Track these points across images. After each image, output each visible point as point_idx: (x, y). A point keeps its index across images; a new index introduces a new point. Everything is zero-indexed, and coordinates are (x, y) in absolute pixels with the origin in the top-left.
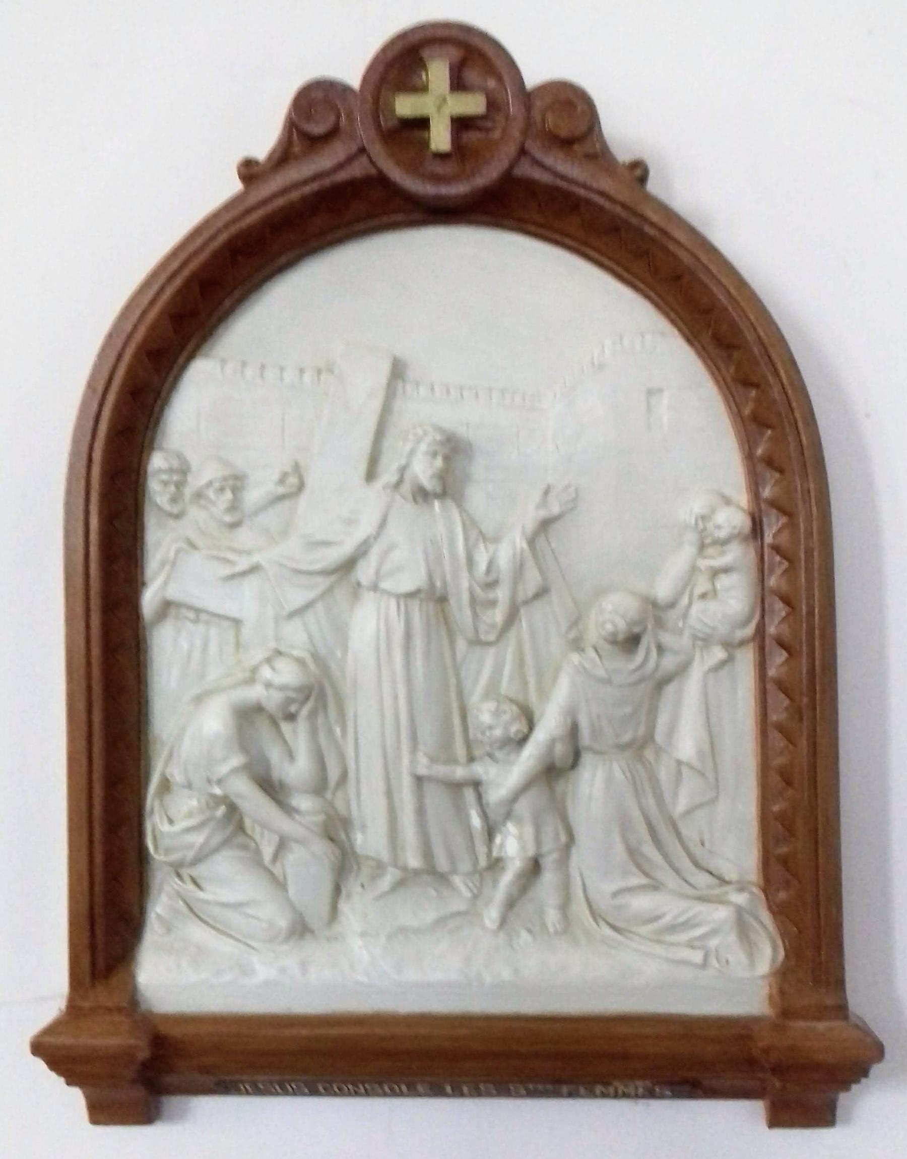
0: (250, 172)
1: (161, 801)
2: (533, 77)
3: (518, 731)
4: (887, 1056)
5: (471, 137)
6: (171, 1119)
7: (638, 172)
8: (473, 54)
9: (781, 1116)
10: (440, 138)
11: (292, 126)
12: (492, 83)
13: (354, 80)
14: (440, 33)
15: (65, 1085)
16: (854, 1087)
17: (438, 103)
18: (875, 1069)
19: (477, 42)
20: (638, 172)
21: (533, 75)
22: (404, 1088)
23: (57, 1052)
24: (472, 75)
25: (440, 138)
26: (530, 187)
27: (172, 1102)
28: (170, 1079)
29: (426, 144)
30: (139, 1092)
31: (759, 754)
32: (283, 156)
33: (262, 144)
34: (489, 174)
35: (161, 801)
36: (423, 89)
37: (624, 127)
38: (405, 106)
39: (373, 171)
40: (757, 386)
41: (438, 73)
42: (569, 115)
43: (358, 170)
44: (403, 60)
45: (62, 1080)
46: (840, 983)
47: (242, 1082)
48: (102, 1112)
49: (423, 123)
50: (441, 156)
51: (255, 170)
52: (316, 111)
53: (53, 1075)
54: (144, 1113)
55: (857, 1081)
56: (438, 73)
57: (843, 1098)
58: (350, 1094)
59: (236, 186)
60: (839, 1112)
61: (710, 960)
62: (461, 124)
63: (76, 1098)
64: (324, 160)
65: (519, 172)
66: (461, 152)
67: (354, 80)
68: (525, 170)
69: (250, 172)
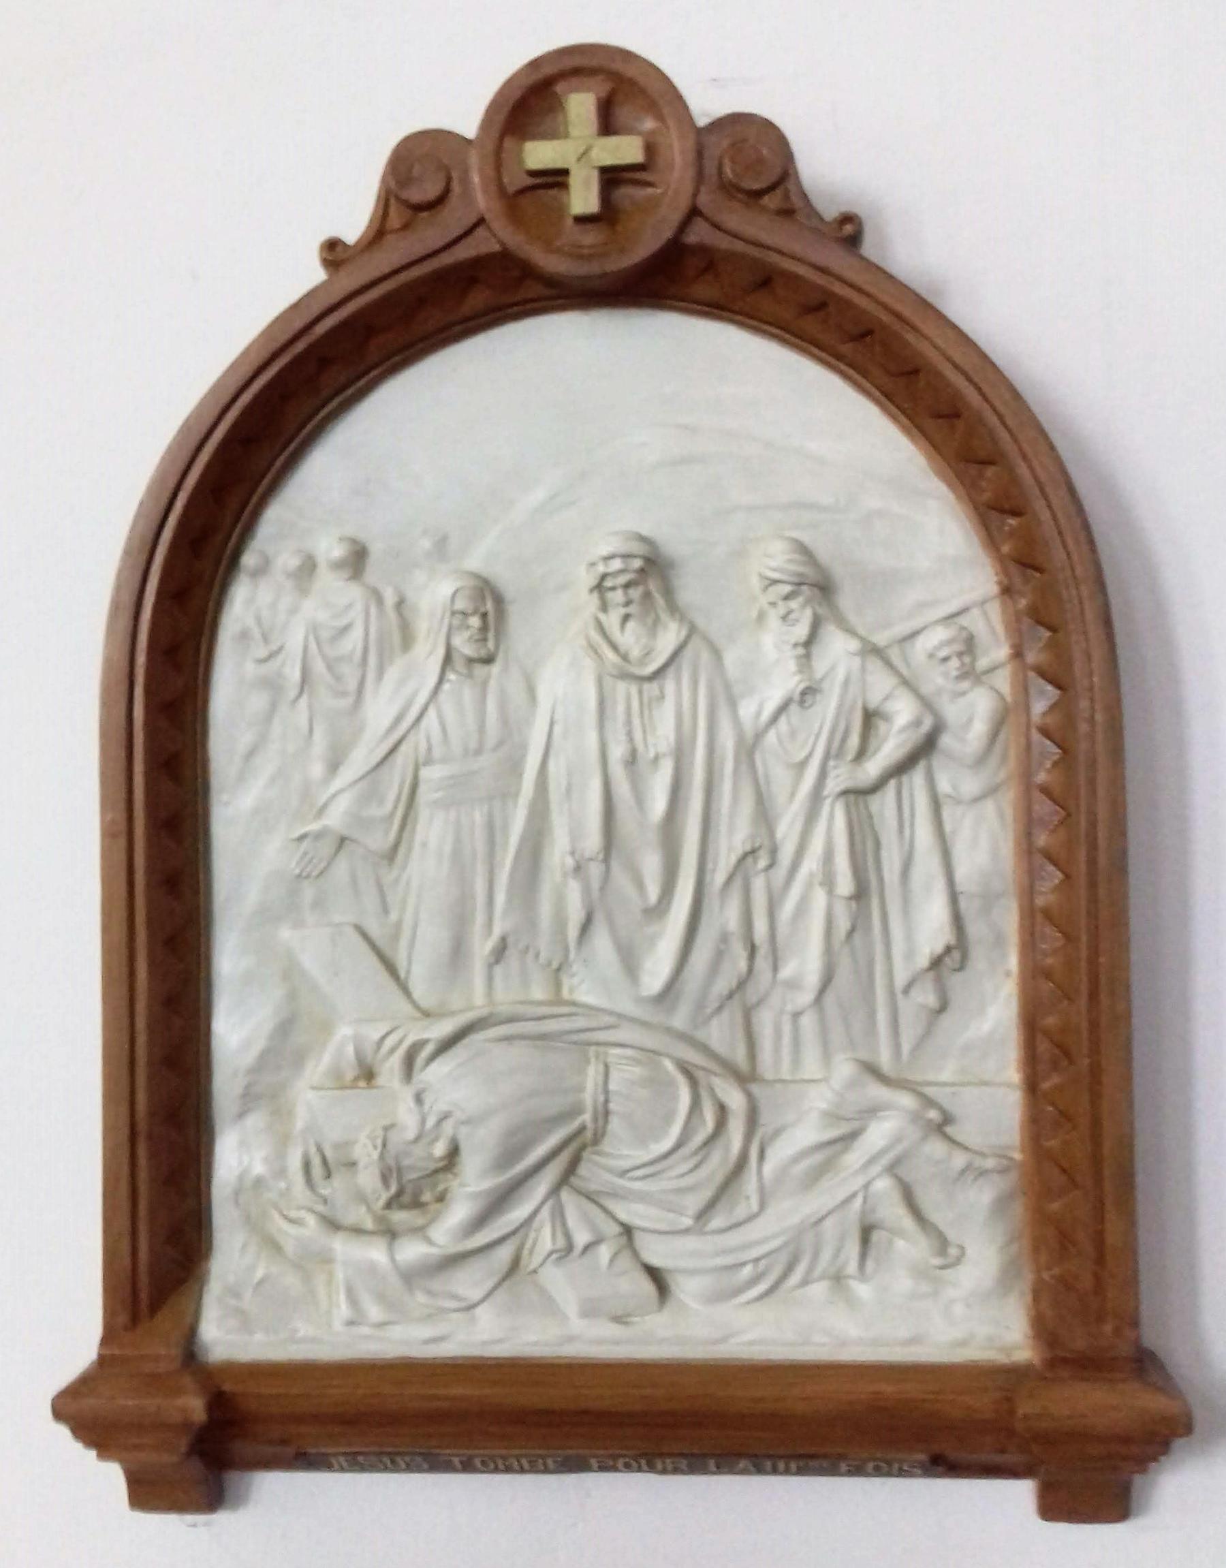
3: (266, 1160)
4: (1198, 1428)
6: (1137, 1515)
7: (849, 229)
8: (622, 84)
9: (1059, 1504)
11: (387, 199)
12: (649, 124)
13: (468, 124)
14: (577, 61)
17: (577, 148)
18: (1178, 1443)
19: (630, 71)
21: (706, 103)
22: (524, 1462)
23: (88, 1413)
24: (623, 114)
25: (583, 197)
26: (703, 250)
27: (233, 1478)
28: (241, 1448)
29: (561, 209)
31: (1137, 977)
32: (378, 234)
33: (353, 225)
34: (645, 243)
37: (830, 166)
38: (540, 154)
40: (1016, 513)
41: (580, 106)
42: (752, 160)
44: (529, 102)
45: (92, 1454)
47: (335, 1455)
48: (147, 1492)
49: (556, 178)
51: (340, 253)
52: (419, 175)
54: (211, 1497)
56: (580, 106)
57: (1138, 1480)
58: (385, 1469)
59: (318, 275)
60: (1134, 1505)
61: (958, 1305)
62: (612, 177)
63: (110, 1478)
64: (430, 235)
66: (607, 216)
67: (468, 124)
68: (699, 234)
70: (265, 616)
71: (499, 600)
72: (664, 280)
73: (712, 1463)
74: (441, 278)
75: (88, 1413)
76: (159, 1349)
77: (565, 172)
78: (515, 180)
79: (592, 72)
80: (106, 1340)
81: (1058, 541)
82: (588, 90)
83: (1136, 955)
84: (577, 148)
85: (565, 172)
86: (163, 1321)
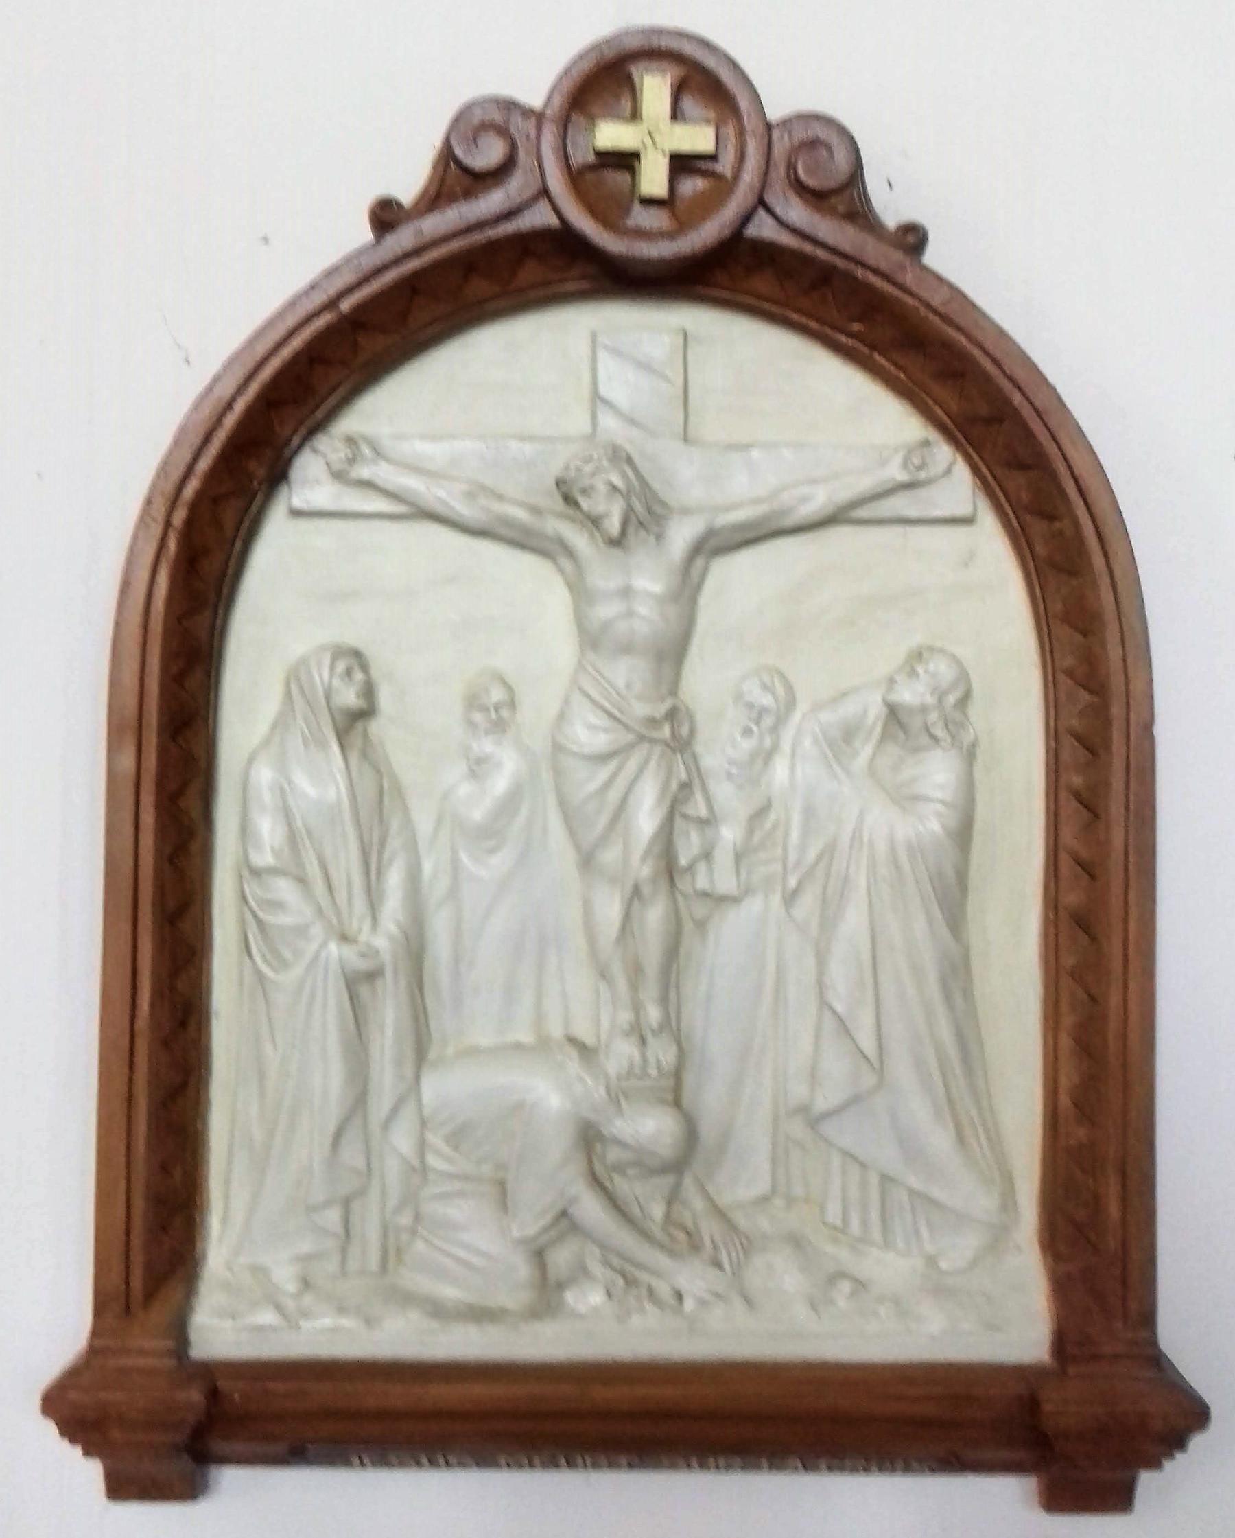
0: (385, 216)
1: (766, 896)
2: (774, 112)
5: (691, 186)
7: (911, 239)
8: (705, 81)
10: (653, 178)
13: (535, 98)
15: (1174, 1462)
16: (1168, 1465)
17: (654, 130)
20: (912, 239)
21: (779, 104)
23: (79, 1409)
25: (653, 178)
28: (218, 1446)
30: (185, 1463)
34: (708, 233)
35: (766, 896)
36: (635, 115)
38: (611, 134)
39: (553, 221)
41: (655, 89)
43: (540, 217)
44: (604, 79)
45: (77, 1451)
46: (1148, 1318)
49: (626, 161)
50: (649, 202)
53: (65, 1444)
54: (187, 1488)
55: (1171, 1456)
56: (655, 89)
59: (365, 234)
61: (1006, 1317)
63: (92, 1472)
65: (752, 231)
68: (763, 228)
69: (385, 216)
70: (304, 580)
71: (357, 654)
72: (732, 273)
73: (765, 1462)
74: (494, 246)
75: (79, 1409)
76: (145, 1346)
77: (635, 156)
78: (581, 156)
79: (676, 58)
80: (95, 1333)
81: (1108, 580)
82: (663, 71)
83: (854, 1470)
84: (654, 130)
85: (635, 156)
86: (159, 1314)
